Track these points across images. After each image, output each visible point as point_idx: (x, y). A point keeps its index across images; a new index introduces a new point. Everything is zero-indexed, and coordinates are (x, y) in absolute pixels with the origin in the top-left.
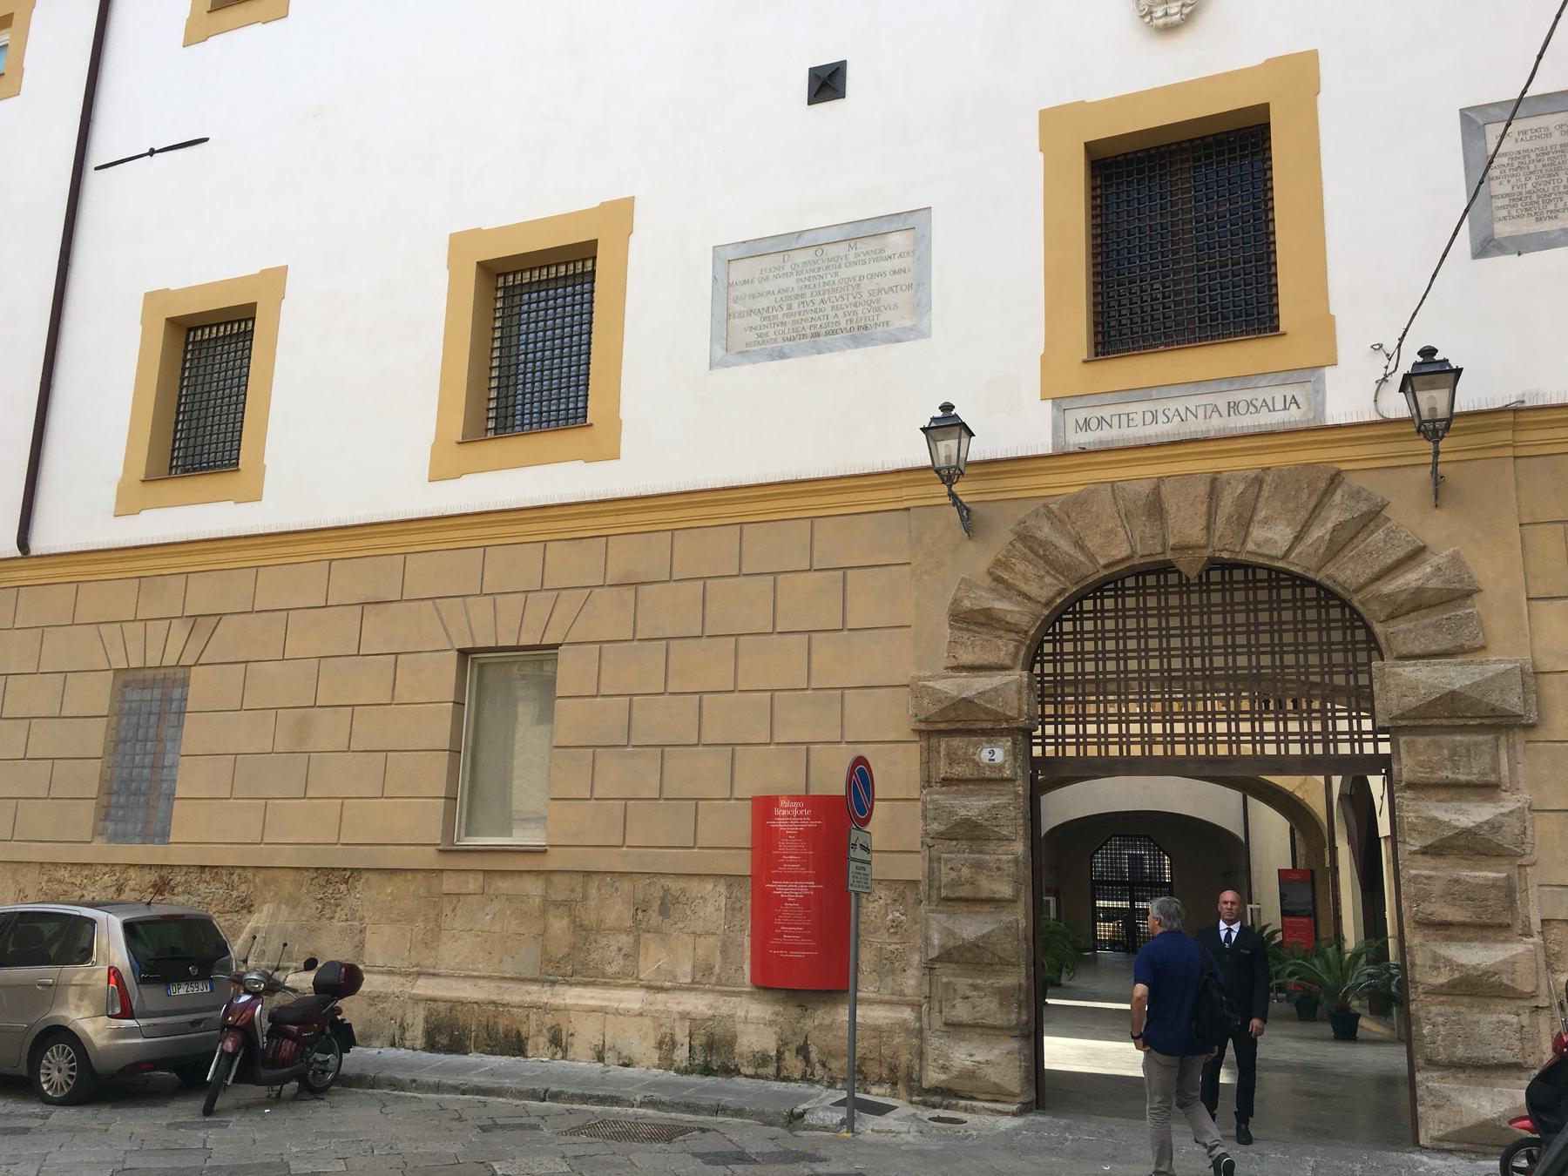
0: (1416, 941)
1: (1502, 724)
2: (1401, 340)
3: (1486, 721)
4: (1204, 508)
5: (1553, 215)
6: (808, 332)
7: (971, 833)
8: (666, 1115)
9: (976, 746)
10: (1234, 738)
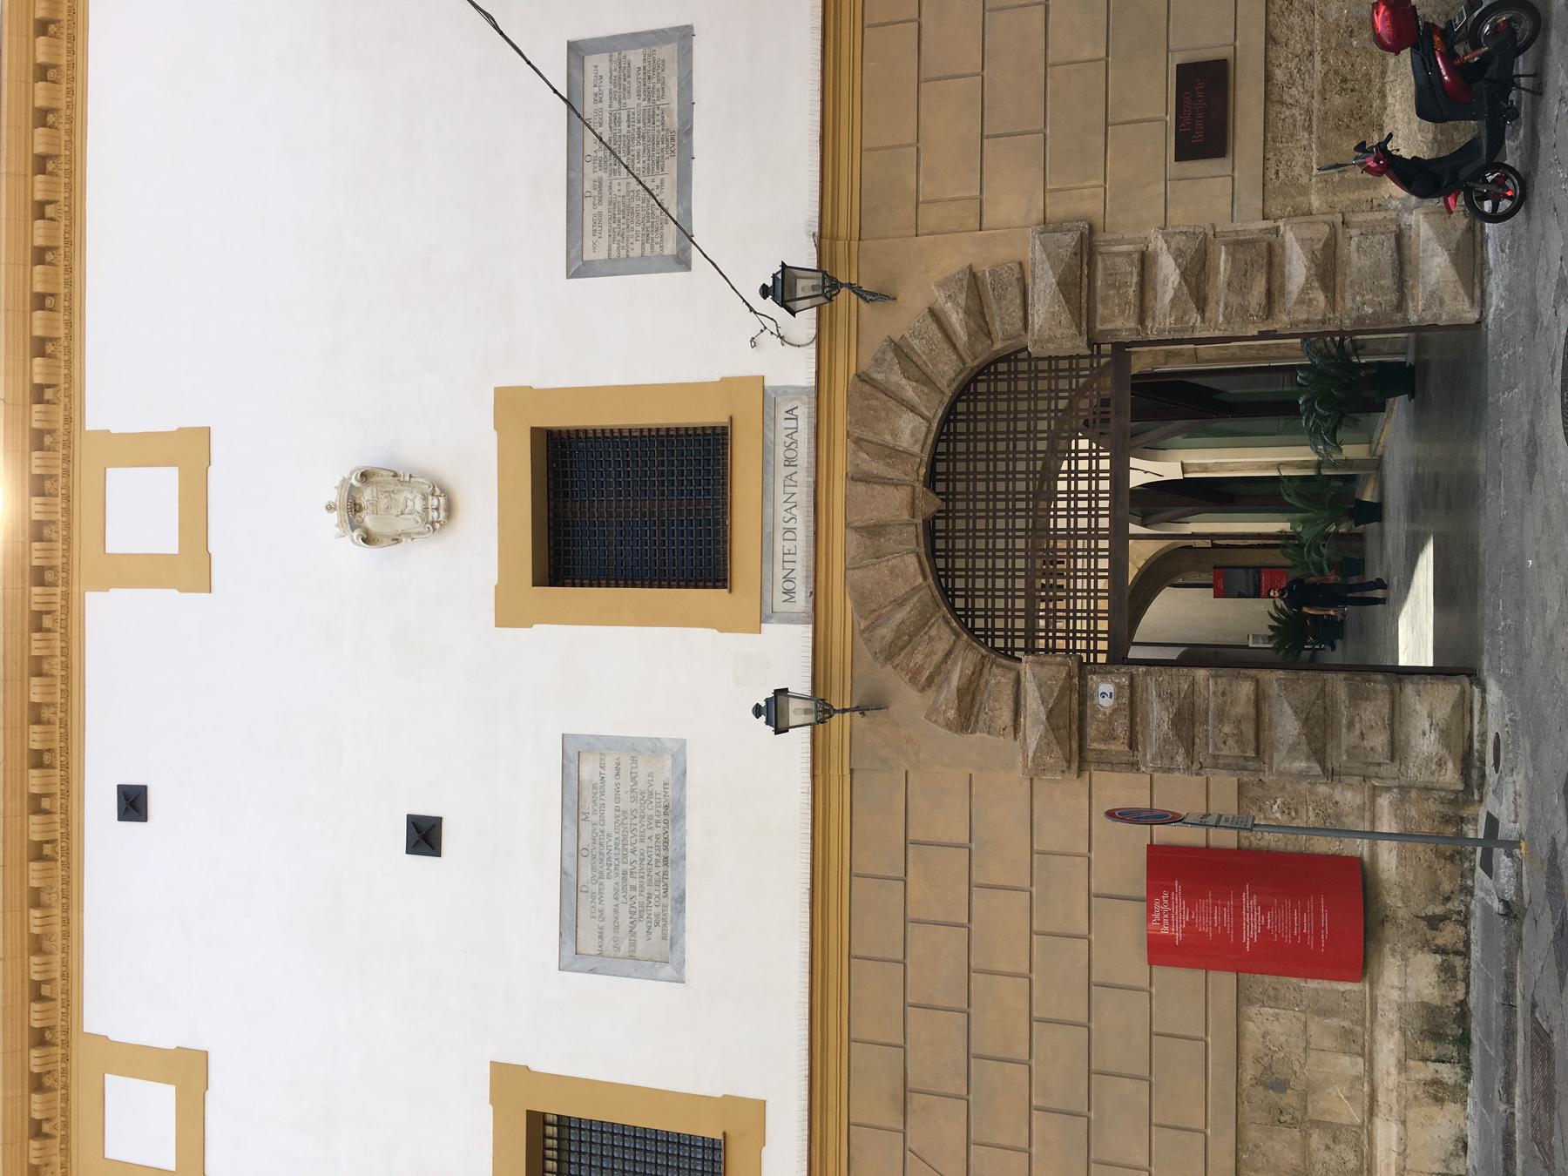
0: (1284, 318)
1: (1088, 246)
2: (751, 310)
4: (878, 487)
6: (661, 869)
7: (1186, 720)
8: (1519, 1076)
9: (1096, 711)
10: (1092, 615)
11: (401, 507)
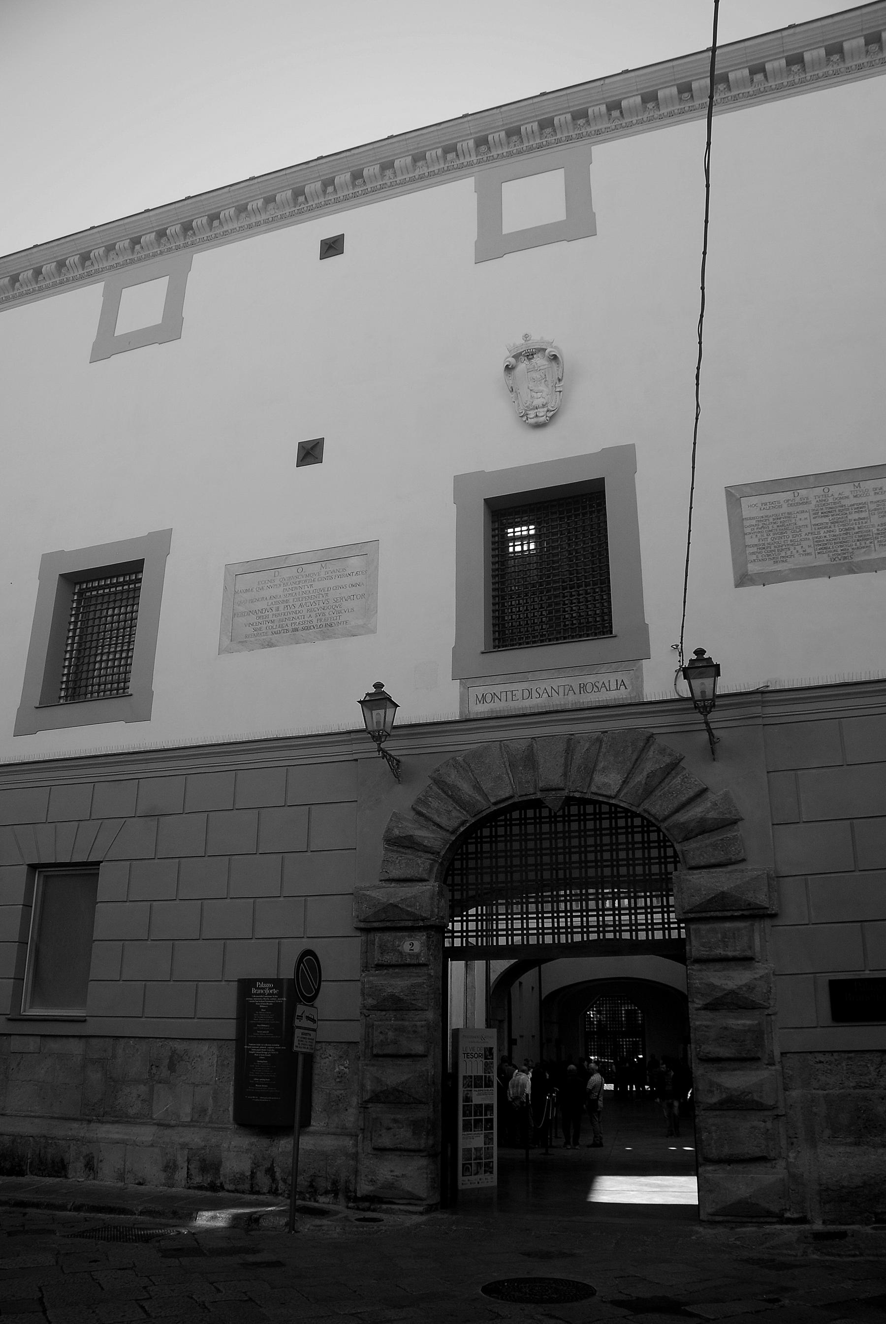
1: (758, 914)
4: (562, 761)
5: (784, 560)
6: (290, 628)
7: (396, 1005)
11: (536, 389)
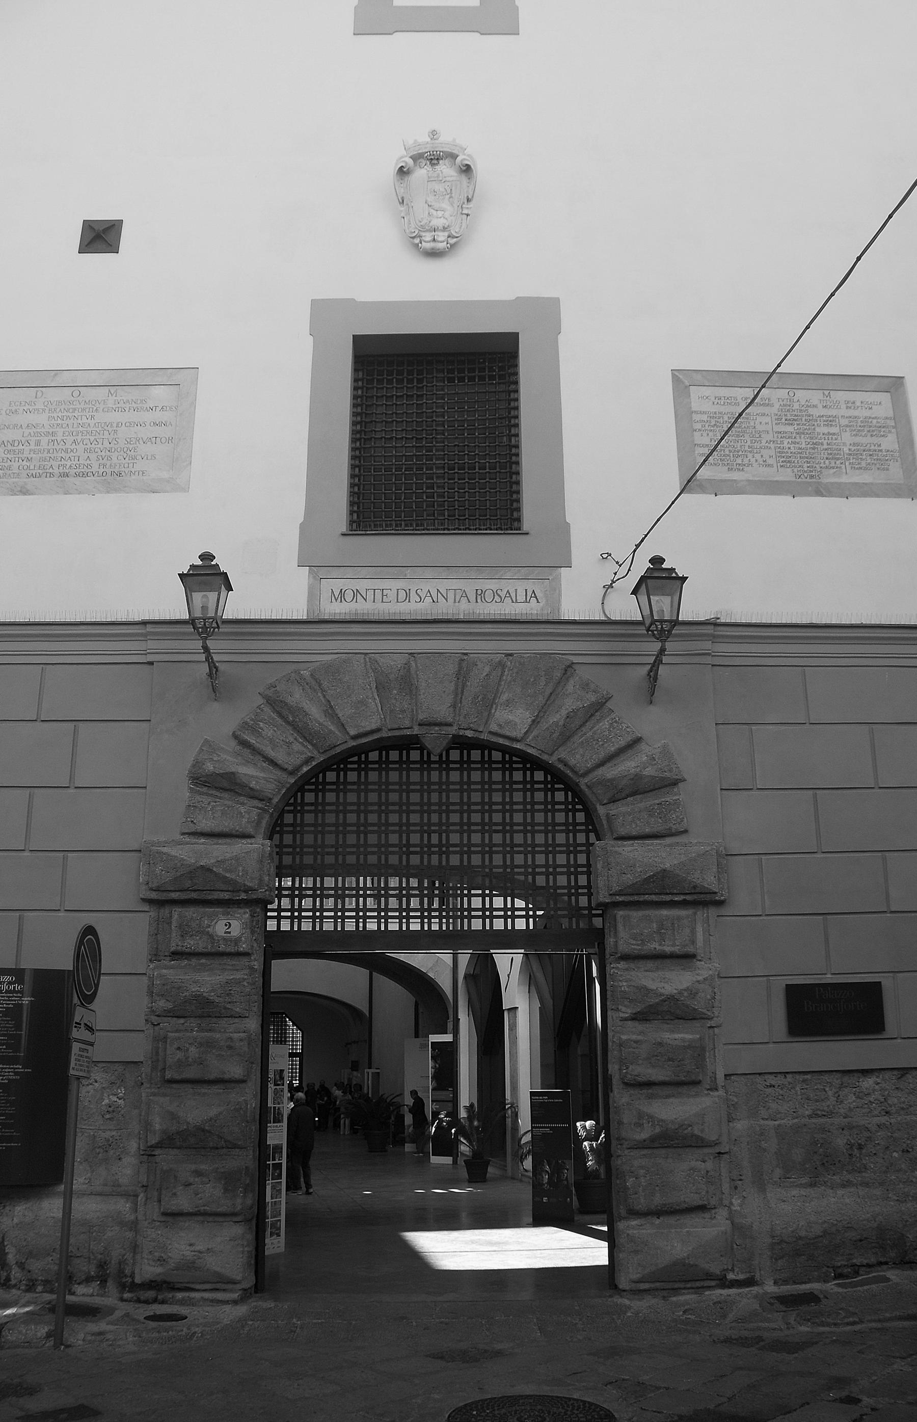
1: (705, 900)
2: (638, 546)
3: (688, 898)
4: (452, 687)
5: (741, 468)
6: (56, 471)
7: (204, 1010)
11: (436, 205)
